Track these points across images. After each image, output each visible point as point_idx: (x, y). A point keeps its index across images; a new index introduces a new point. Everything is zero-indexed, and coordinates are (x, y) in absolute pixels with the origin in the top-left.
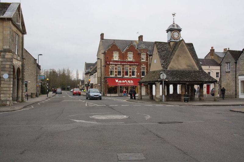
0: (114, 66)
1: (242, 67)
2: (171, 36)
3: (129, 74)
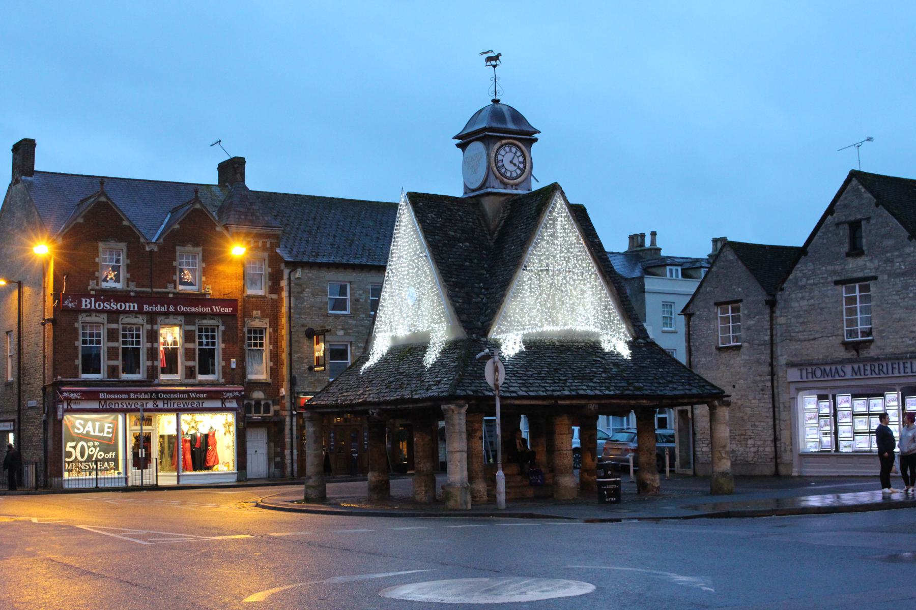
0: (103, 318)
1: (803, 323)
2: (489, 168)
3: (104, 363)
